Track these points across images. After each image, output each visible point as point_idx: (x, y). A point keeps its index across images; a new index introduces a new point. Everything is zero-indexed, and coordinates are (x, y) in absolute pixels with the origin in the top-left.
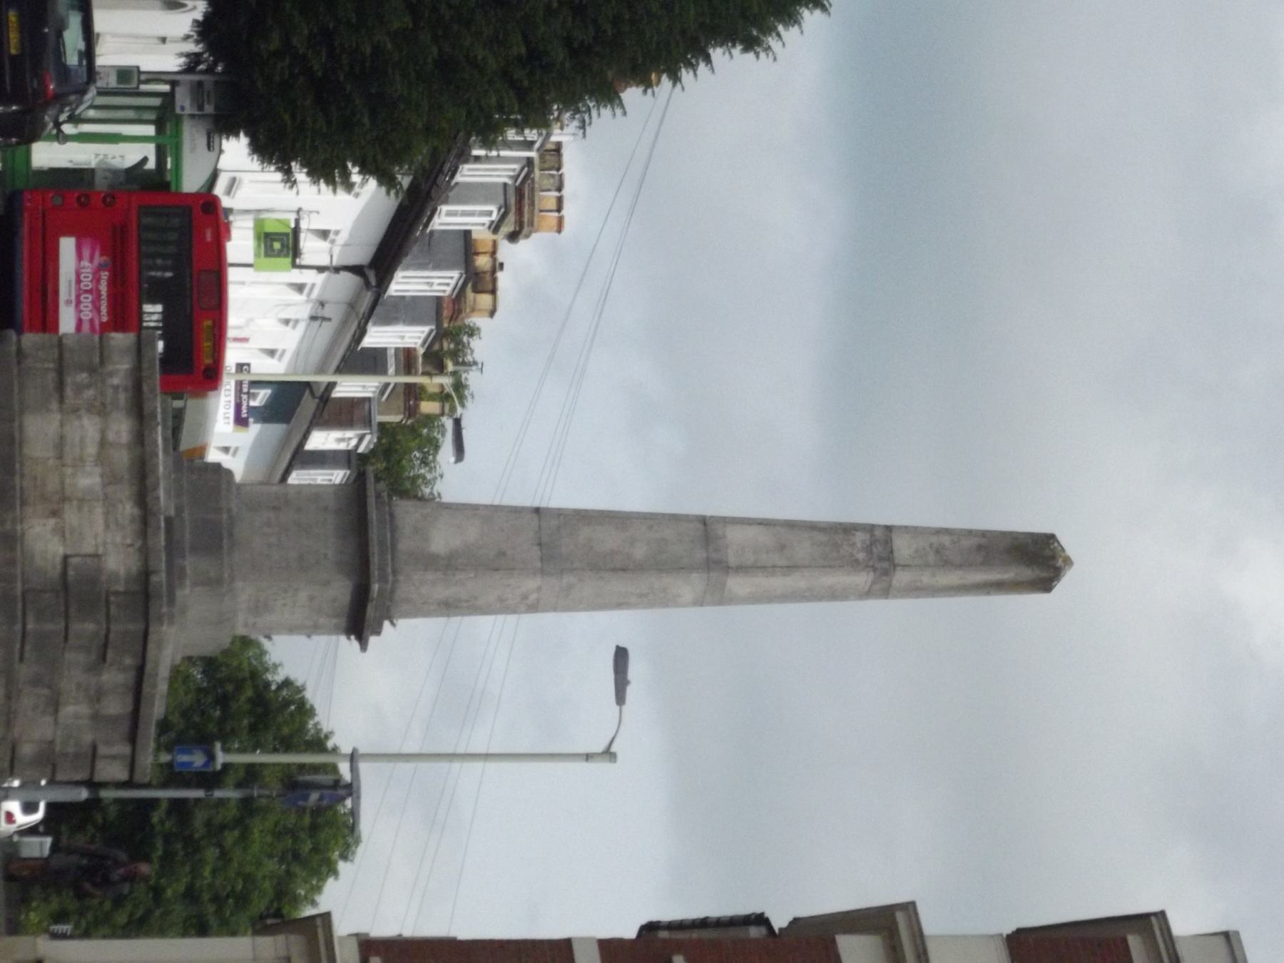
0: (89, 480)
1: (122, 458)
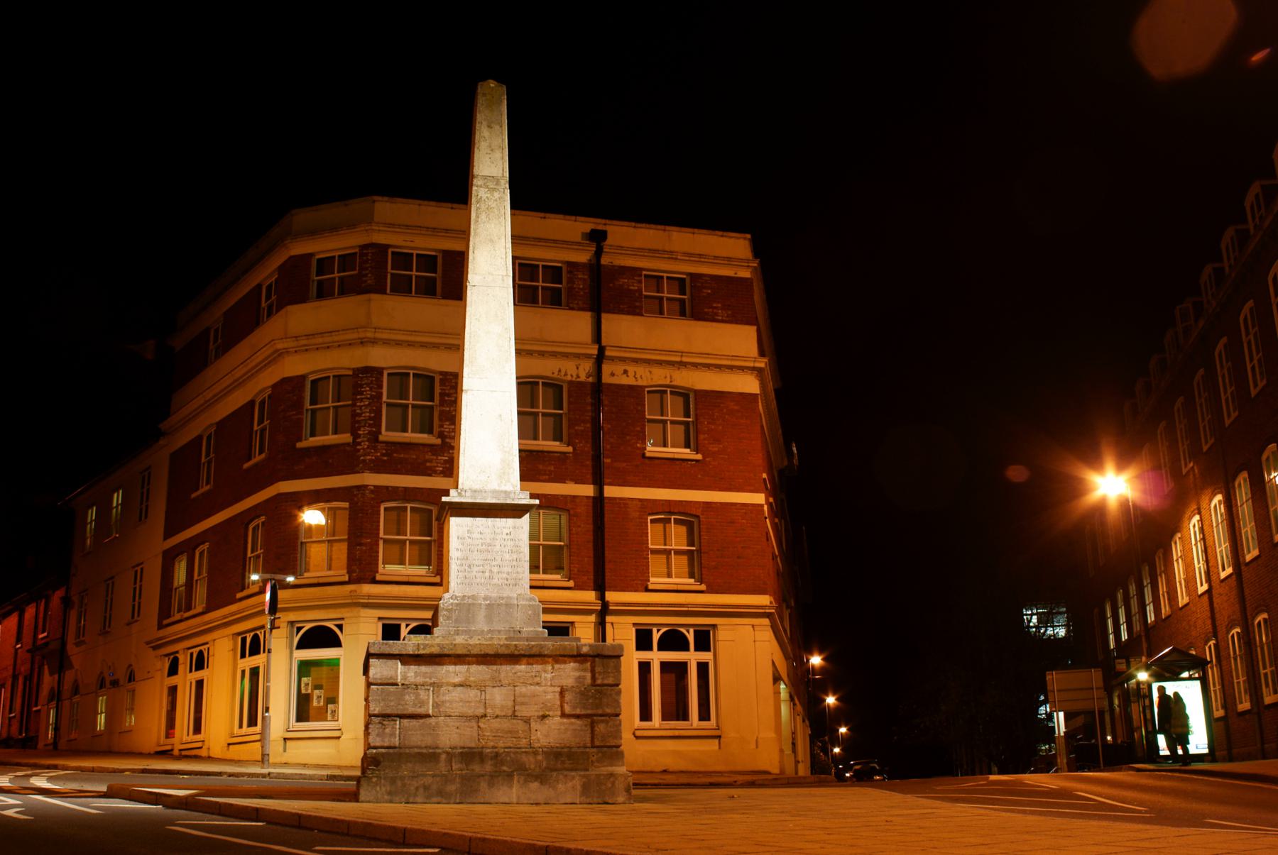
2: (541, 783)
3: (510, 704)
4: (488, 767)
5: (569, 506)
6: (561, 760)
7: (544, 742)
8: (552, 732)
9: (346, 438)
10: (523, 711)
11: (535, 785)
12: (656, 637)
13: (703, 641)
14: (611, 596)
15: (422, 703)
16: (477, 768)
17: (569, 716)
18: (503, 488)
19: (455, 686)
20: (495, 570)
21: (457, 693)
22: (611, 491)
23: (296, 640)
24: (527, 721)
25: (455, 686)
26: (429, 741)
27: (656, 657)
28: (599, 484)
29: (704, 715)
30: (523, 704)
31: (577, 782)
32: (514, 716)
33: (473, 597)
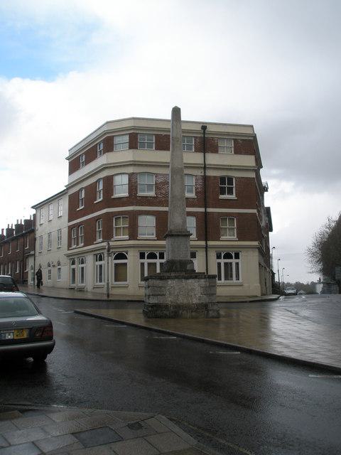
14: (210, 243)
22: (210, 210)
27: (223, 261)
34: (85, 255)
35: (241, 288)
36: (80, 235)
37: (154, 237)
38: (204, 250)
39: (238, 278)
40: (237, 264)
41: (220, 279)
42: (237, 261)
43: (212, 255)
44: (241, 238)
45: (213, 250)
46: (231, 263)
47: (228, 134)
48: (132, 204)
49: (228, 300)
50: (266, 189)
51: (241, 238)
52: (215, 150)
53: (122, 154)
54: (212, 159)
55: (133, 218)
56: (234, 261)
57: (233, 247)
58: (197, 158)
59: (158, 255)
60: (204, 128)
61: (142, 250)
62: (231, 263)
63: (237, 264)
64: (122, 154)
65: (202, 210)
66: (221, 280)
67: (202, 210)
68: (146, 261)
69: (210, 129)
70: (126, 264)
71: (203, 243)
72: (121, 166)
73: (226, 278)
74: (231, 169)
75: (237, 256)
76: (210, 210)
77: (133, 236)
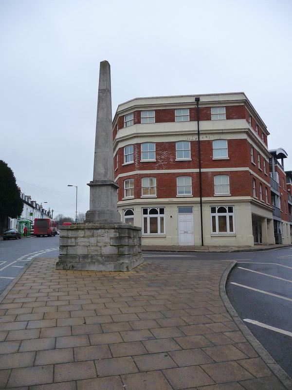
0: (93, 240)
1: (88, 233)
2: (103, 265)
3: (96, 242)
4: (89, 260)
5: (191, 175)
6: (109, 258)
7: (105, 253)
8: (108, 250)
9: (133, 162)
10: (99, 244)
11: (101, 266)
12: (217, 209)
13: (231, 210)
14: (204, 199)
15: (72, 242)
16: (86, 260)
17: (112, 246)
18: (105, 180)
19: (81, 237)
20: (102, 203)
21: (82, 239)
22: (203, 170)
23: (124, 213)
24: (100, 247)
25: (81, 237)
26: (75, 253)
27: (217, 215)
28: (200, 169)
29: (231, 230)
30: (99, 242)
31: (113, 265)
32: (97, 246)
33: (95, 211)
34: (134, 207)
35: (234, 239)
36: (125, 188)
37: (191, 194)
38: (200, 205)
39: (231, 230)
40: (162, 219)
41: (146, 231)
42: (162, 215)
43: (207, 209)
44: (233, 193)
45: (207, 205)
46: (225, 217)
47: (219, 102)
48: (160, 167)
49: (237, 249)
50: (7, 164)
51: (233, 193)
52: (208, 118)
53: (183, 125)
54: (205, 125)
55: (138, 179)
56: (159, 216)
57: (225, 202)
58: (192, 126)
59: (159, 211)
60: (197, 100)
61: (145, 206)
62: (225, 217)
63: (162, 219)
64: (183, 125)
65: (197, 170)
66: (163, 232)
67: (197, 170)
68: (149, 216)
69: (202, 100)
70: (133, 219)
71: (198, 199)
72: (182, 135)
73: (220, 230)
74: (222, 133)
75: (162, 211)
76: (203, 170)
77: (138, 195)
